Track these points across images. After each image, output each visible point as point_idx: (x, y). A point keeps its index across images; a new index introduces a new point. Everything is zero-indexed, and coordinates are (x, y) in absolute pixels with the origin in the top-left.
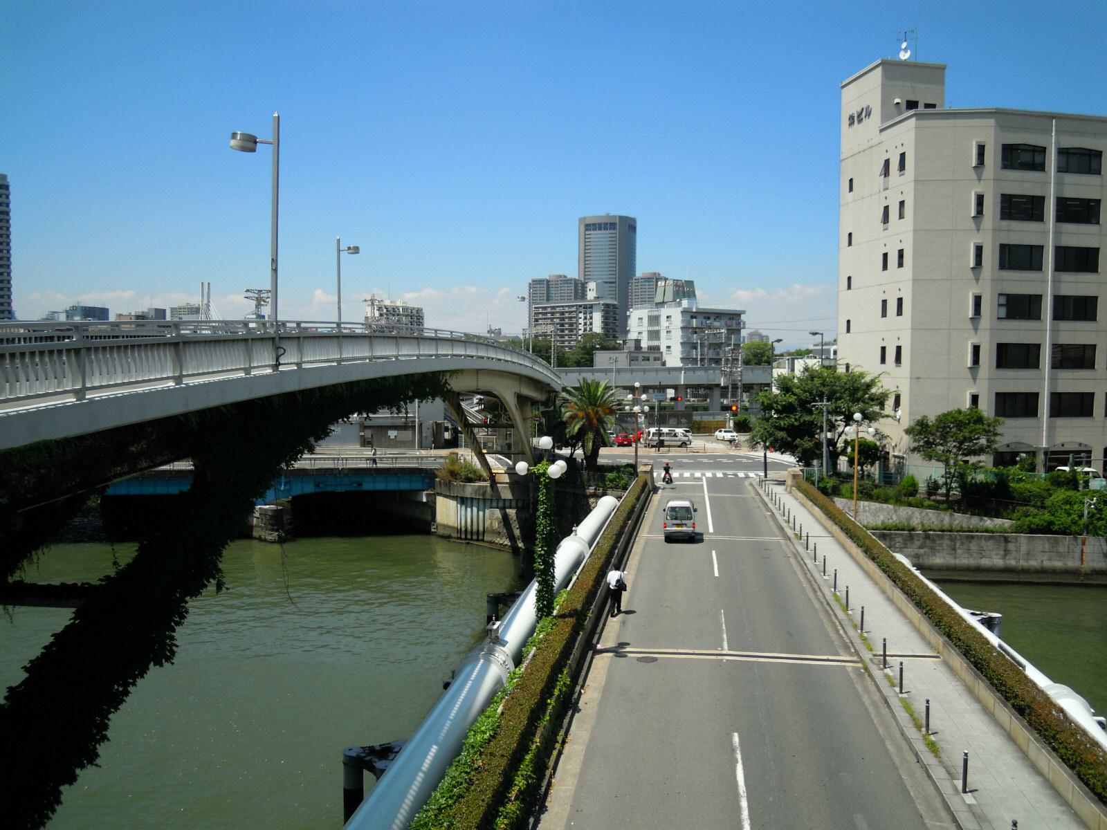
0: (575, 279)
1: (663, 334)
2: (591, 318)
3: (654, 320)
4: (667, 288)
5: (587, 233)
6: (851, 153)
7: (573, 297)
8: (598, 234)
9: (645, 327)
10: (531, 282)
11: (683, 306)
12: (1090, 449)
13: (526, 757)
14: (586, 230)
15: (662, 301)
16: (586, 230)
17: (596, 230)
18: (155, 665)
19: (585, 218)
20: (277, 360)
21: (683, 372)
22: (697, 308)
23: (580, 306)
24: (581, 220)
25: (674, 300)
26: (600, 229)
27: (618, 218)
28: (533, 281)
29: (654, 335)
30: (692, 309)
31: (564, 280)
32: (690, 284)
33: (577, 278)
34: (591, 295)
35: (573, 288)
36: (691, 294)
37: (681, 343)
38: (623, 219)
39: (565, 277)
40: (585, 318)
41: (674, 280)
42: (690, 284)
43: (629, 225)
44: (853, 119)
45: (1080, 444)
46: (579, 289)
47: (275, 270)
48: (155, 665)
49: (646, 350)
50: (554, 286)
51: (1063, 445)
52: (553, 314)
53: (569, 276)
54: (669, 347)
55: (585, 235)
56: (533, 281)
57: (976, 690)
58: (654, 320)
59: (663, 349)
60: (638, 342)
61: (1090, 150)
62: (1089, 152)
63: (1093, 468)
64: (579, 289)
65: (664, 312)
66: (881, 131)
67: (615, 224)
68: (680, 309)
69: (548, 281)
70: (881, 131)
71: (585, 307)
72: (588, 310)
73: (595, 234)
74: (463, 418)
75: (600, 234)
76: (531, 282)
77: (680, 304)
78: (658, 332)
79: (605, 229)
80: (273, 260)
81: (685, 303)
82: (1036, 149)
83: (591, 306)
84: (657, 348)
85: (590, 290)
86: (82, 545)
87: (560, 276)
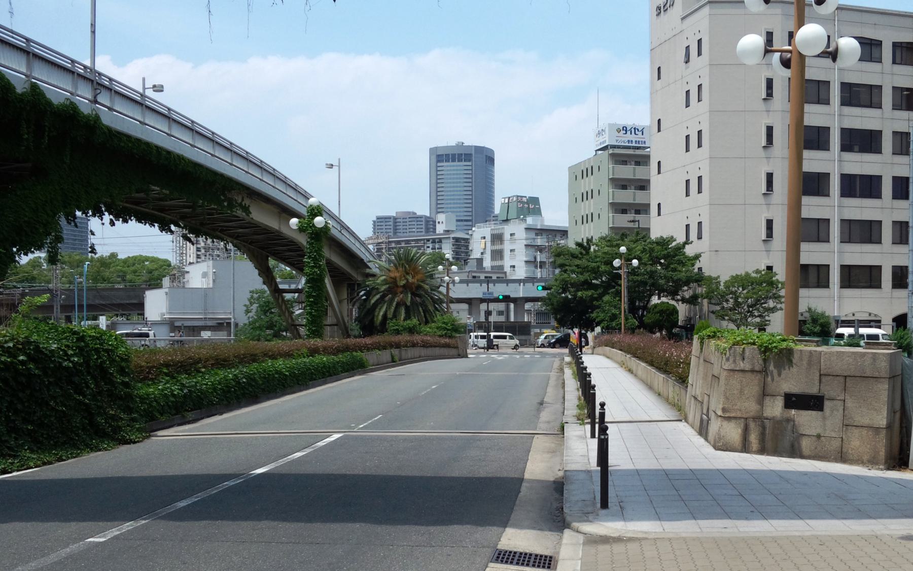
0: (426, 217)
1: (507, 254)
3: (497, 238)
4: (510, 204)
5: (439, 164)
6: (659, 43)
7: (423, 230)
8: (450, 166)
10: (375, 219)
11: (528, 223)
12: (879, 319)
14: (438, 161)
15: (506, 219)
16: (438, 161)
17: (449, 161)
20: (95, 97)
21: (522, 284)
22: (541, 225)
23: (428, 240)
24: (433, 151)
25: (518, 218)
26: (453, 161)
27: (473, 148)
28: (378, 218)
29: (498, 255)
30: (537, 225)
31: (414, 218)
32: (535, 201)
33: (428, 215)
34: (440, 229)
35: (423, 226)
36: (537, 212)
37: (526, 262)
38: (480, 150)
39: (415, 214)
41: (518, 196)
42: (535, 201)
43: (486, 156)
44: (660, 10)
45: (870, 314)
46: (430, 224)
47: (93, 32)
49: (490, 270)
50: (401, 224)
51: (854, 315)
53: (419, 213)
55: (437, 167)
56: (378, 218)
58: (497, 238)
59: (507, 269)
60: (480, 261)
61: (872, 40)
62: (870, 42)
63: (884, 330)
64: (430, 224)
65: (507, 230)
66: (683, 19)
67: (471, 155)
68: (524, 226)
69: (395, 219)
70: (683, 19)
71: (434, 241)
72: (437, 246)
73: (448, 166)
74: (273, 284)
75: (453, 166)
76: (375, 219)
77: (524, 220)
79: (459, 161)
80: (92, 24)
81: (530, 220)
82: (873, 42)
83: (440, 241)
84: (501, 267)
85: (439, 223)
87: (409, 213)
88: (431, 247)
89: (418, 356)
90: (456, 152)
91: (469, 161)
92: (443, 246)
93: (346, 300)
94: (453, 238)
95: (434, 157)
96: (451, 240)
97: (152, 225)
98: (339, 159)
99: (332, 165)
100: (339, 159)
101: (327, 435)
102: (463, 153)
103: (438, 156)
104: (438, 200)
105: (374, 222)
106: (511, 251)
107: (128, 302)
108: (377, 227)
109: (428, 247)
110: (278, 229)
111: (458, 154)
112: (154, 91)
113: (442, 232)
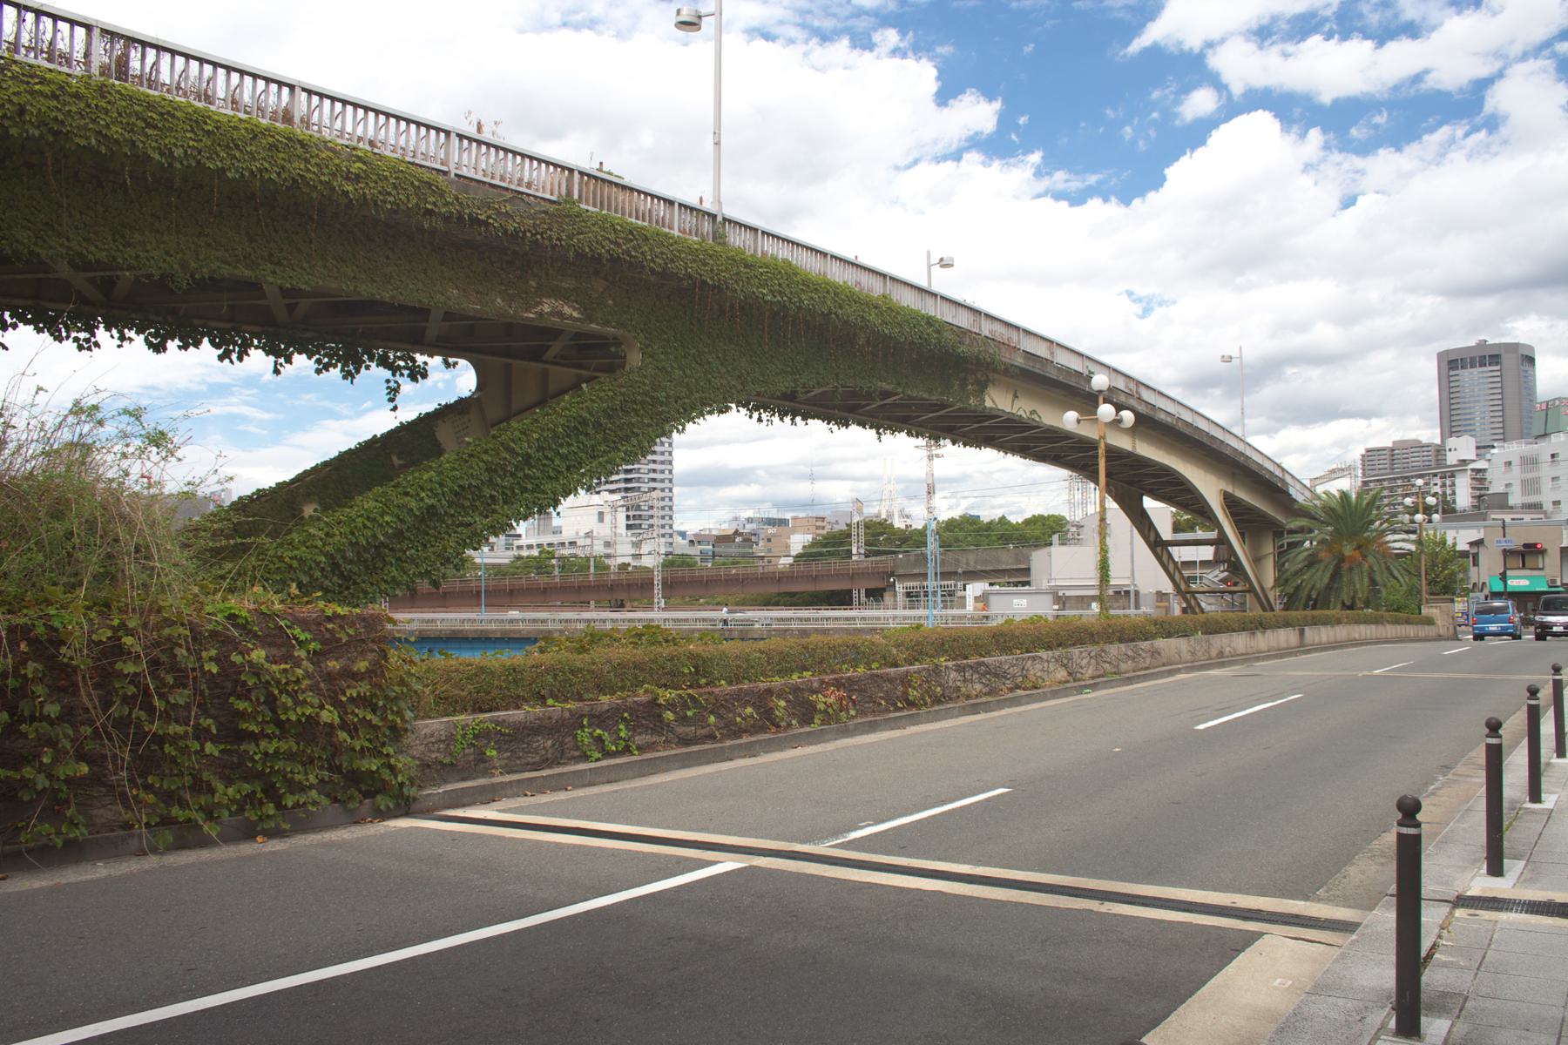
1: (1547, 485)
2: (1453, 484)
5: (1452, 373)
9: (1516, 475)
10: (1364, 452)
13: (522, 528)
16: (1451, 369)
17: (1485, 365)
18: (377, 366)
19: (1447, 352)
23: (1435, 475)
39: (1420, 442)
40: (1444, 485)
48: (377, 366)
52: (1391, 489)
53: (1425, 440)
54: (1557, 503)
57: (82, 51)
59: (1548, 506)
72: (1448, 482)
76: (1364, 452)
78: (1537, 481)
79: (1480, 366)
86: (1256, 908)
88: (1439, 484)
89: (1266, 649)
90: (1477, 354)
91: (1497, 364)
92: (1457, 481)
93: (1272, 556)
94: (1473, 470)
95: (1445, 365)
96: (1469, 472)
97: (724, 410)
98: (1241, 348)
99: (1231, 358)
100: (1241, 348)
101: (902, 851)
102: (1487, 354)
103: (1450, 362)
104: (1451, 421)
105: (1363, 456)
106: (1554, 479)
107: (1015, 567)
108: (1367, 467)
109: (1436, 484)
110: (1130, 449)
111: (1480, 357)
112: (941, 266)
113: (1455, 462)
